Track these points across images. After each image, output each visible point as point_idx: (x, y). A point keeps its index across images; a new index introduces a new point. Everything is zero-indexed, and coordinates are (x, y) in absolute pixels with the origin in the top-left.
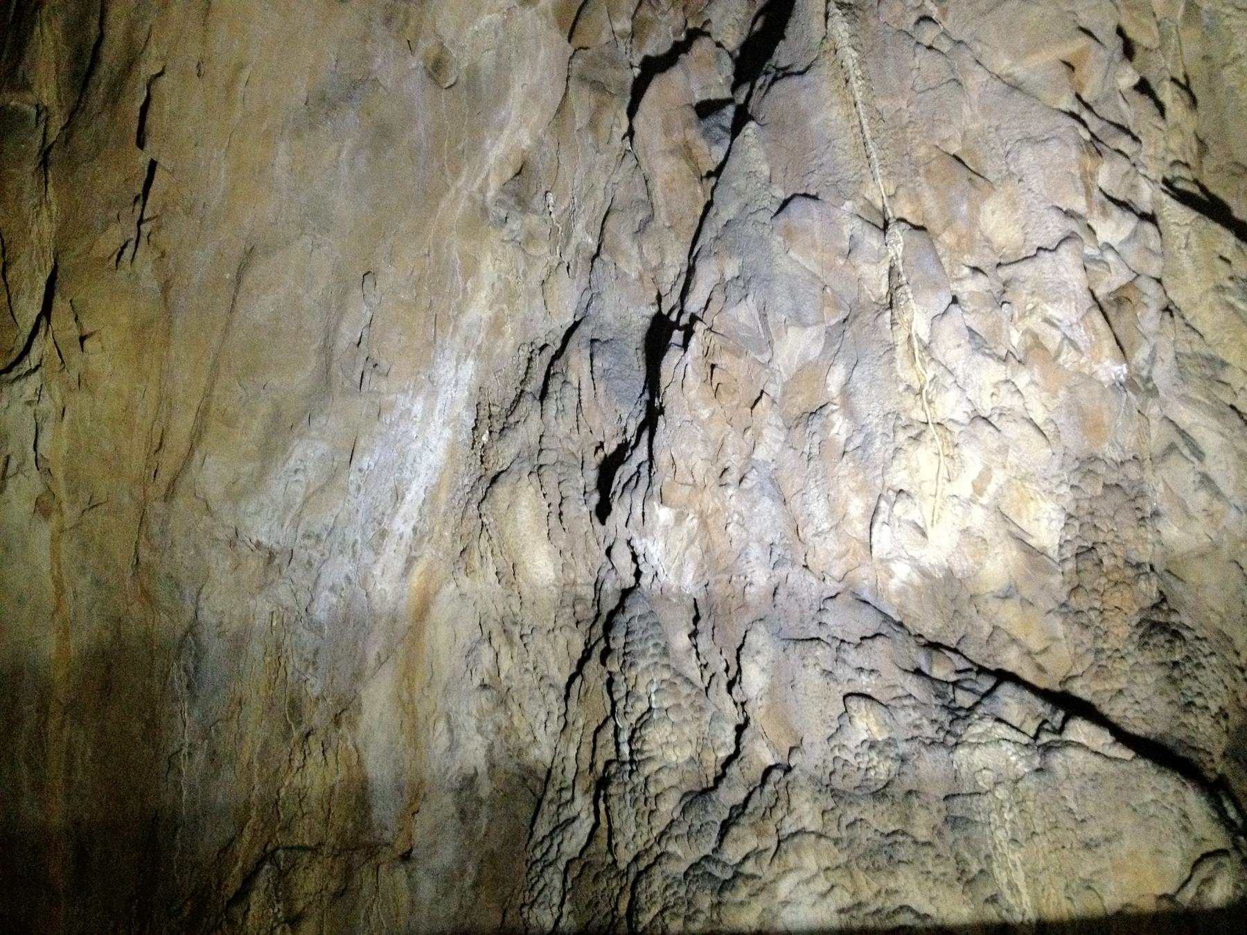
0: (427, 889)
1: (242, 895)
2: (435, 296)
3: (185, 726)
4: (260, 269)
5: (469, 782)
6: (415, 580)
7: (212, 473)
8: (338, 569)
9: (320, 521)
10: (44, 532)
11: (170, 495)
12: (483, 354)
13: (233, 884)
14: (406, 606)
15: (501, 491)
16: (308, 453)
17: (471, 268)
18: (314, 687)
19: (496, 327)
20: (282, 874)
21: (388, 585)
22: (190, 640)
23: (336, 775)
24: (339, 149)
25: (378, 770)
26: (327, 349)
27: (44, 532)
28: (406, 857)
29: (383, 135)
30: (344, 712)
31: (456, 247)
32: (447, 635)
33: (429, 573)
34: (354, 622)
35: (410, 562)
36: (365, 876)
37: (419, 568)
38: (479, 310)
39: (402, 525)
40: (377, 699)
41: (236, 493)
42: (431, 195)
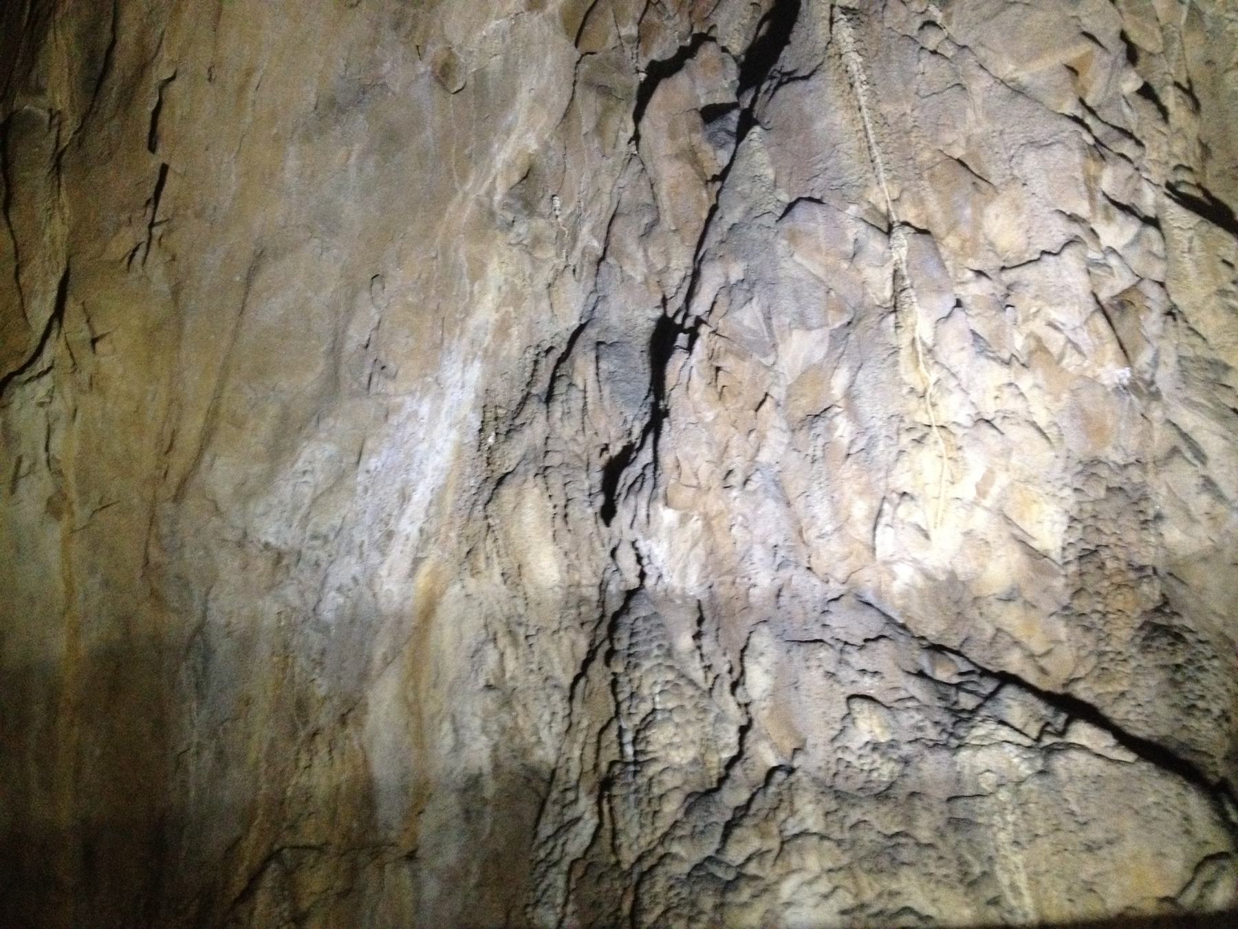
0: (431, 889)
1: (248, 894)
2: (443, 297)
3: (193, 725)
4: (270, 272)
5: (473, 782)
6: (422, 580)
7: (221, 474)
8: (346, 570)
9: (326, 522)
10: (55, 532)
11: (179, 497)
12: (490, 356)
13: (239, 883)
14: (413, 605)
15: (507, 492)
16: (316, 454)
17: (478, 271)
18: (321, 687)
19: (502, 330)
20: (288, 873)
21: (394, 585)
22: (199, 640)
23: (343, 774)
24: (349, 153)
25: (384, 770)
26: (335, 351)
27: (55, 532)
28: (411, 857)
29: (391, 139)
30: (350, 711)
31: (463, 252)
32: (453, 635)
33: (435, 574)
34: (360, 623)
35: (417, 562)
36: (369, 875)
37: (425, 569)
38: (486, 313)
39: (421, 495)
40: (383, 699)
41: (245, 494)
42: (437, 200)
